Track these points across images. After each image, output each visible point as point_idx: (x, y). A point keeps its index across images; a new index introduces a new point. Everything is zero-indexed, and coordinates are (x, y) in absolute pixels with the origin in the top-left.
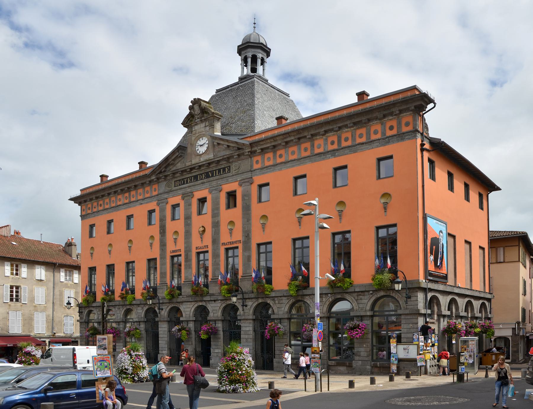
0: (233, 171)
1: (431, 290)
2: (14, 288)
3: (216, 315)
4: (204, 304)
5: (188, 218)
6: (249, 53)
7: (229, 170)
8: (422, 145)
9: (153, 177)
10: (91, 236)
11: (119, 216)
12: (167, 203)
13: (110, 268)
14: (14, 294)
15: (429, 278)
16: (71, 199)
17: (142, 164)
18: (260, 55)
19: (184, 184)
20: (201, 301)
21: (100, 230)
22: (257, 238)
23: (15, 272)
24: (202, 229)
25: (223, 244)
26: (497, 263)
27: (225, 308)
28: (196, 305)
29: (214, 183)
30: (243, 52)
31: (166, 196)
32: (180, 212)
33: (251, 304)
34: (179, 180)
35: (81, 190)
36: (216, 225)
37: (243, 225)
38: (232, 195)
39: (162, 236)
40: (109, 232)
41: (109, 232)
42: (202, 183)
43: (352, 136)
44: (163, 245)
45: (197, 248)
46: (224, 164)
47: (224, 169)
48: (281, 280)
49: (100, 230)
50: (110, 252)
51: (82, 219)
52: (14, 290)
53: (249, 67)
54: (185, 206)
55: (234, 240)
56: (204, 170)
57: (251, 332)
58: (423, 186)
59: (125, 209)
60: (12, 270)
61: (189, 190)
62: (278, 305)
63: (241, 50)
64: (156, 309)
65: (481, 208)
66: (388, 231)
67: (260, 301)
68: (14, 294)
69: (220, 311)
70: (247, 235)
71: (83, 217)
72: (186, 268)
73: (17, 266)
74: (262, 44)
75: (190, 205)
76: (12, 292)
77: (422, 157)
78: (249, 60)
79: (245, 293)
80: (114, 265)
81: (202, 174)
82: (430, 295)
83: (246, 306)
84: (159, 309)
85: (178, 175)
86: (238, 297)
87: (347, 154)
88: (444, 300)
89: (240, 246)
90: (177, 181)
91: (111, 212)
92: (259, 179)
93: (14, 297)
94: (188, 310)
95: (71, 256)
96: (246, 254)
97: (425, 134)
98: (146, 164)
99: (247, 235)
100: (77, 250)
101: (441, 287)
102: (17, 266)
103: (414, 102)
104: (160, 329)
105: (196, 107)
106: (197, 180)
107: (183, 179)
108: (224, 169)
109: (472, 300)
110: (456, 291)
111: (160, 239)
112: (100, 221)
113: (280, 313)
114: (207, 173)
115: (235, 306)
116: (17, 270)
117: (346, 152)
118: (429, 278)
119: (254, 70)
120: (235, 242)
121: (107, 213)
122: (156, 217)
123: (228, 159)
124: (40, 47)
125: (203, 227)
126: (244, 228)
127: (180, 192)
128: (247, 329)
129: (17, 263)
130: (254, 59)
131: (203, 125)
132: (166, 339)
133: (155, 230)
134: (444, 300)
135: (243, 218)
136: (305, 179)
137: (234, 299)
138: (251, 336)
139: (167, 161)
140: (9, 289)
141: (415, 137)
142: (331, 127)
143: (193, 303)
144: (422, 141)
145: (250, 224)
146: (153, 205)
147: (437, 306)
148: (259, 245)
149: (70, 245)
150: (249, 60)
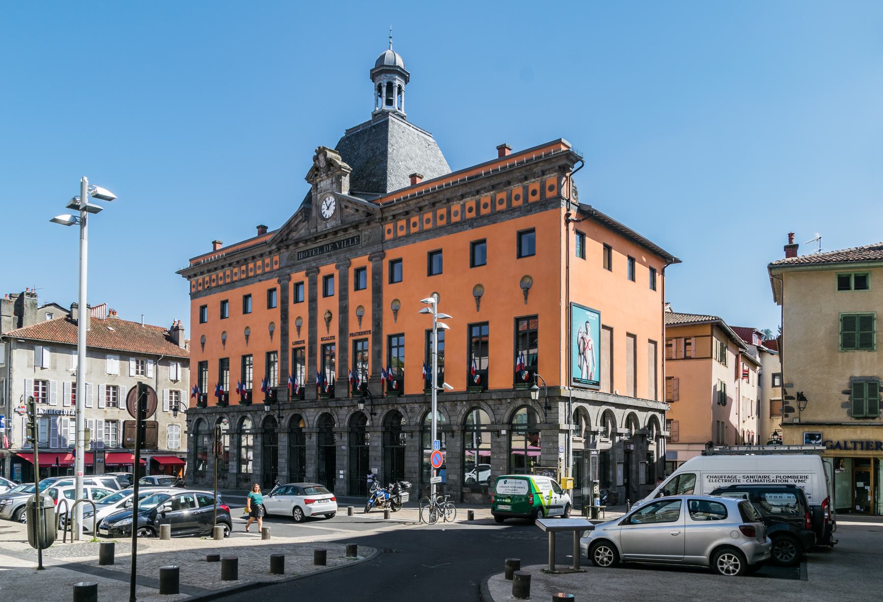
0: (363, 241)
1: (575, 400)
2: (40, 383)
3: (342, 425)
4: (328, 410)
5: (313, 300)
6: (384, 80)
7: (359, 240)
8: (568, 215)
9: (274, 247)
10: (202, 321)
11: (235, 296)
13: (224, 364)
14: (40, 392)
15: (574, 384)
16: (179, 273)
18: (398, 81)
20: (326, 407)
21: (213, 312)
22: (388, 329)
23: (140, 370)
24: (328, 315)
25: (352, 335)
26: (686, 358)
27: (352, 417)
28: (320, 413)
29: (342, 256)
30: (377, 78)
32: (304, 293)
33: (381, 412)
35: (190, 260)
36: (344, 310)
37: (374, 311)
40: (223, 317)
41: (223, 317)
45: (322, 339)
46: (352, 233)
47: (353, 239)
49: (213, 312)
50: (224, 342)
51: (192, 299)
52: (40, 385)
53: (384, 99)
54: (309, 285)
55: (363, 330)
56: (330, 239)
57: (380, 448)
58: (568, 268)
60: (137, 367)
64: (276, 417)
65: (654, 288)
66: (528, 325)
67: (391, 408)
69: (348, 416)
70: (378, 323)
71: (194, 296)
73: (142, 363)
74: (399, 67)
77: (567, 230)
78: (384, 90)
79: (375, 398)
80: (228, 359)
81: (328, 245)
82: (575, 405)
83: (375, 414)
84: (279, 417)
85: (301, 244)
86: (367, 403)
87: (486, 225)
88: (595, 413)
89: (370, 337)
92: (392, 254)
93: (40, 396)
94: (311, 417)
95: (177, 343)
96: (377, 348)
97: (572, 200)
98: (266, 228)
99: (378, 323)
100: (185, 336)
101: (590, 395)
102: (142, 363)
103: (560, 161)
104: (279, 443)
105: (321, 158)
106: (323, 252)
109: (636, 412)
110: (612, 399)
112: (213, 301)
114: (334, 243)
115: (363, 414)
116: (142, 368)
117: (485, 222)
118: (574, 384)
119: (389, 102)
120: (365, 333)
122: (277, 298)
125: (329, 312)
126: (374, 315)
127: (304, 267)
128: (376, 444)
129: (143, 359)
130: (390, 86)
133: (276, 314)
134: (595, 413)
135: (373, 302)
137: (361, 406)
138: (380, 454)
139: (289, 227)
140: (71, 388)
141: (559, 206)
142: (468, 190)
143: (317, 410)
144: (568, 210)
145: (381, 310)
147: (586, 419)
148: (390, 337)
149: (176, 329)
150: (384, 90)
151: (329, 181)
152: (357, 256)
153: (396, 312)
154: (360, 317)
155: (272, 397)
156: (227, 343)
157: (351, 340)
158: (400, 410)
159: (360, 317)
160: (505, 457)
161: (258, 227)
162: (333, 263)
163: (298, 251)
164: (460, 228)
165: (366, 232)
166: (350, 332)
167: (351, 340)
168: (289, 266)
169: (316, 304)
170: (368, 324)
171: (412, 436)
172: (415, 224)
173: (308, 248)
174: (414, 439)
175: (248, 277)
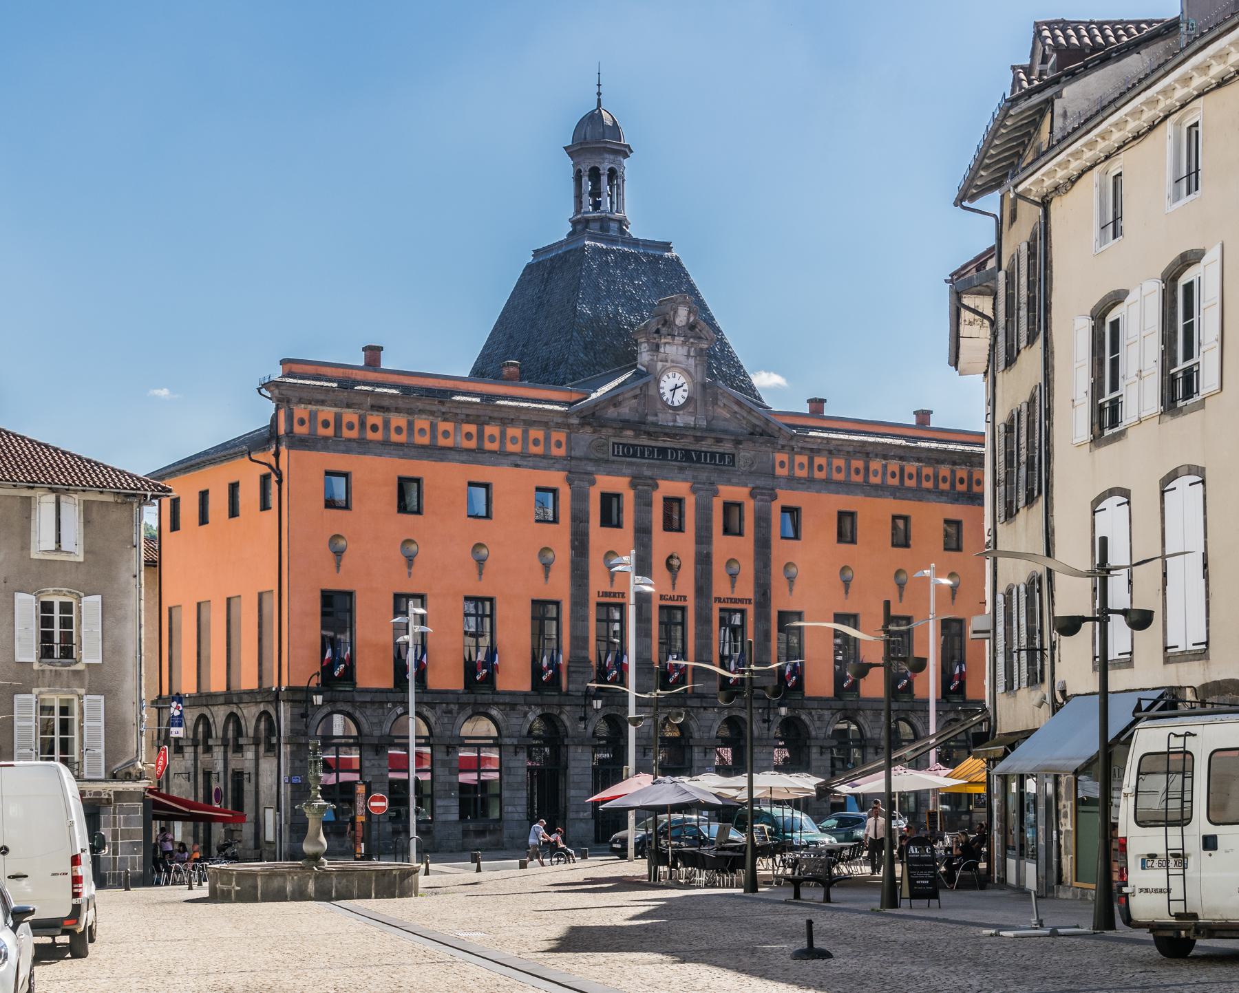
14: (57, 630)
19: (634, 456)
25: (719, 600)
29: (703, 476)
34: (624, 445)
36: (704, 560)
38: (610, 502)
39: (577, 555)
43: (546, 439)
44: (580, 575)
46: (727, 447)
47: (722, 455)
48: (819, 682)
59: (463, 462)
68: (57, 630)
72: (585, 640)
75: (649, 504)
76: (47, 622)
81: (676, 450)
89: (750, 610)
90: (618, 444)
92: (787, 497)
106: (665, 458)
107: (633, 446)
111: (573, 562)
120: (741, 601)
124: (1119, 148)
126: (757, 578)
135: (756, 560)
145: (769, 573)
151: (683, 351)
152: (729, 482)
153: (791, 580)
154: (733, 576)
155: (545, 682)
156: (346, 560)
157: (716, 607)
158: (803, 717)
159: (733, 576)
160: (525, 794)
161: (364, 349)
162: (685, 480)
163: (616, 440)
164: (880, 493)
165: (745, 454)
166: (715, 595)
167: (716, 607)
168: (597, 461)
169: (650, 540)
170: (746, 589)
171: (821, 753)
172: (820, 468)
173: (636, 442)
174: (824, 757)
175: (480, 450)
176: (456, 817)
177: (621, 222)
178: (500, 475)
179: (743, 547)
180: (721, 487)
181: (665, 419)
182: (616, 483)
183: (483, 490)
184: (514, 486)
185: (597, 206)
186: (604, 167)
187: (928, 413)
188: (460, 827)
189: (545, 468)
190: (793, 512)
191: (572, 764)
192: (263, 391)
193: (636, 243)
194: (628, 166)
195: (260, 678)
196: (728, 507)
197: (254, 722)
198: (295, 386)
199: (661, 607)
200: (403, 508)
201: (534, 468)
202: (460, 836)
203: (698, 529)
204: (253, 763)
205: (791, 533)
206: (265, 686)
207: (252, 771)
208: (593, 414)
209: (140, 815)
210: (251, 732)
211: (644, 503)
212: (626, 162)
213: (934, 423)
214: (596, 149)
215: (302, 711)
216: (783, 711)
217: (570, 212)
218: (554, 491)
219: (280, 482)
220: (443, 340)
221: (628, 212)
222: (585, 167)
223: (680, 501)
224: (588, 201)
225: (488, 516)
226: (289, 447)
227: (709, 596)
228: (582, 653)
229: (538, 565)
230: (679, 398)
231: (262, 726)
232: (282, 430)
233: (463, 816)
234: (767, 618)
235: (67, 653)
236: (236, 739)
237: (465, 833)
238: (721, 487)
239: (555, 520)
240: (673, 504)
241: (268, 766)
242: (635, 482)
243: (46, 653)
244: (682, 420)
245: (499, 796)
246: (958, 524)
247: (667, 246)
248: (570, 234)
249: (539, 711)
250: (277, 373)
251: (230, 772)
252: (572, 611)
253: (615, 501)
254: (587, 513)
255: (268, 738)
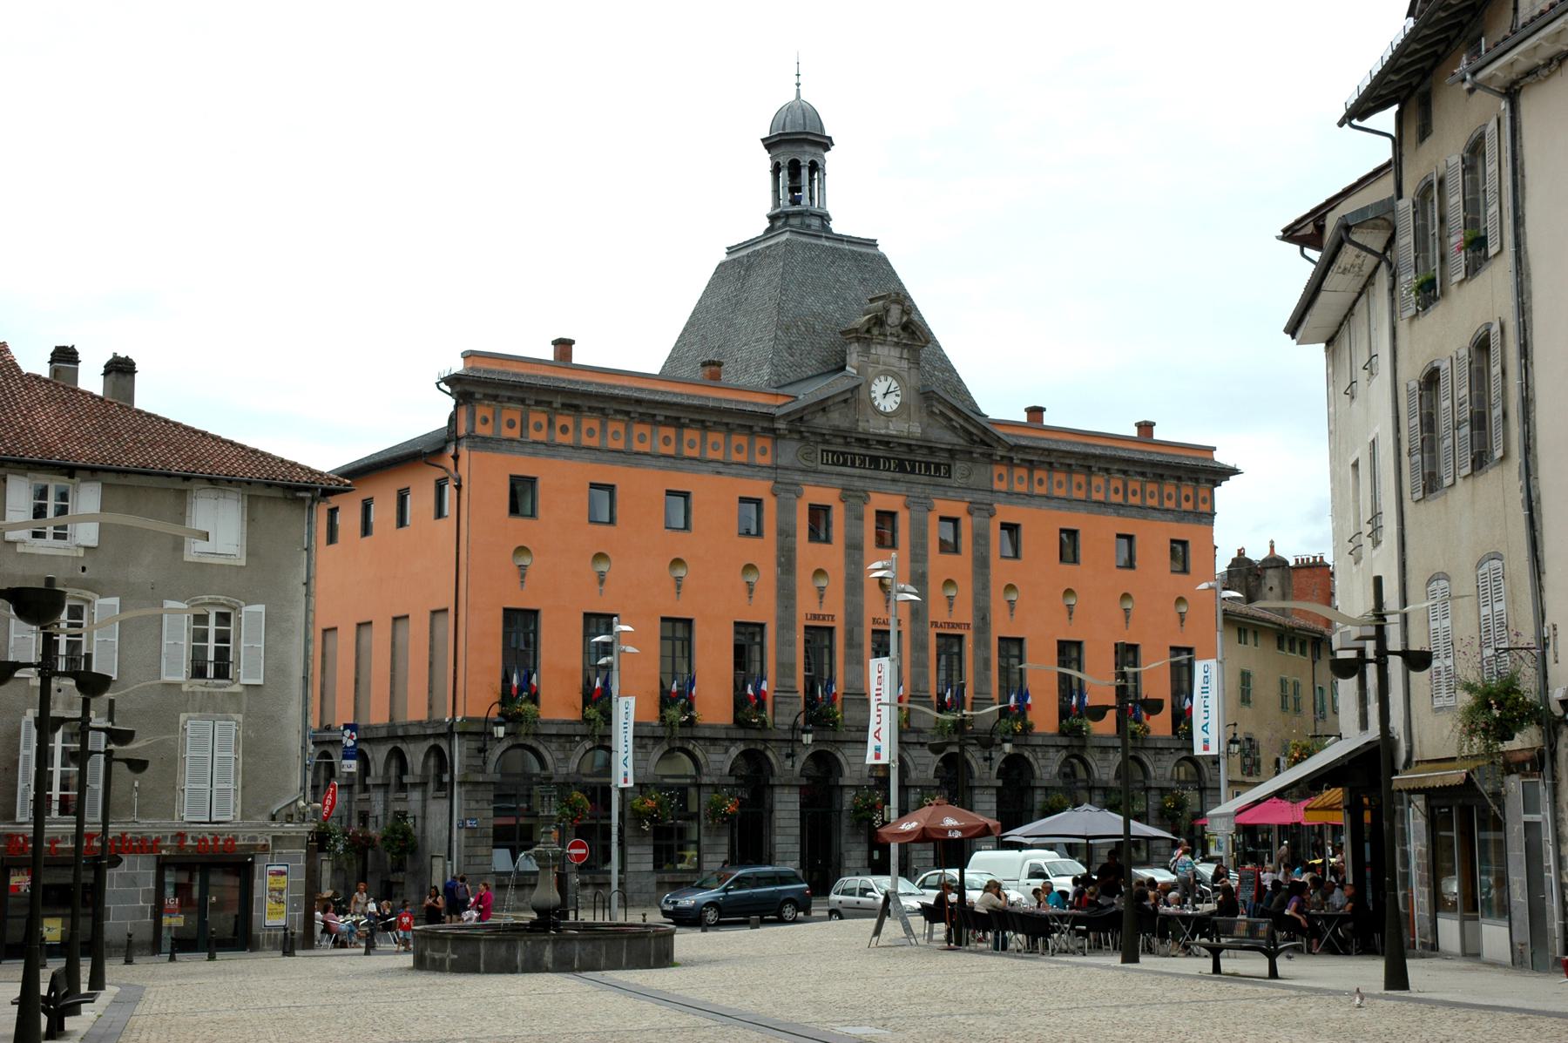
12: (799, 496)
17: (564, 346)
19: (845, 464)
25: (935, 624)
29: (918, 490)
31: (798, 477)
34: (834, 453)
35: (468, 355)
42: (893, 480)
44: (786, 595)
46: (941, 458)
47: (938, 466)
48: (1044, 716)
59: (660, 468)
61: (858, 484)
62: (1042, 762)
63: (770, 144)
68: (211, 644)
72: (793, 666)
75: (860, 518)
81: (889, 459)
91: (605, 462)
92: (1008, 512)
106: (877, 468)
107: (843, 454)
108: (938, 466)
111: (778, 580)
113: (1046, 776)
120: (959, 625)
121: (592, 461)
123: (952, 453)
126: (975, 600)
131: (895, 352)
132: (778, 839)
136: (394, 523)
146: (759, 488)
158: (1026, 754)
166: (931, 619)
169: (862, 556)
170: (964, 613)
176: (650, 867)
177: (824, 218)
178: (698, 483)
179: (960, 566)
180: (936, 502)
181: (875, 427)
182: (825, 495)
183: (606, 494)
184: (716, 497)
185: (795, 201)
186: (805, 161)
187: (1040, 410)
188: (654, 879)
189: (748, 477)
190: (1011, 529)
191: (778, 806)
192: (442, 385)
193: (840, 239)
194: (832, 160)
195: (430, 707)
196: (881, 515)
197: (421, 758)
198: (478, 385)
199: (874, 631)
200: (514, 509)
201: (737, 475)
202: (653, 889)
203: (913, 546)
204: (419, 804)
205: (1009, 552)
206: (437, 717)
207: (419, 813)
208: (801, 419)
209: (302, 864)
210: (418, 769)
211: (786, 509)
212: (827, 155)
213: (1048, 420)
214: (797, 148)
215: (480, 744)
216: (1008, 747)
217: (767, 206)
218: (758, 502)
219: (459, 488)
220: (634, 335)
221: (831, 208)
222: (784, 161)
223: (826, 509)
224: (785, 195)
225: (612, 521)
226: (470, 448)
227: (924, 621)
228: (788, 682)
229: (741, 582)
230: (889, 404)
231: (432, 762)
232: (462, 431)
233: (658, 866)
234: (987, 646)
235: (222, 672)
236: (400, 778)
237: (661, 885)
238: (936, 502)
239: (759, 534)
240: (886, 518)
241: (437, 808)
242: (847, 494)
243: (198, 672)
244: (893, 429)
245: (698, 842)
246: (1072, 534)
247: (872, 243)
248: (768, 231)
249: (742, 747)
250: (458, 366)
251: (390, 814)
252: (778, 634)
253: (822, 514)
254: (794, 526)
255: (439, 777)
